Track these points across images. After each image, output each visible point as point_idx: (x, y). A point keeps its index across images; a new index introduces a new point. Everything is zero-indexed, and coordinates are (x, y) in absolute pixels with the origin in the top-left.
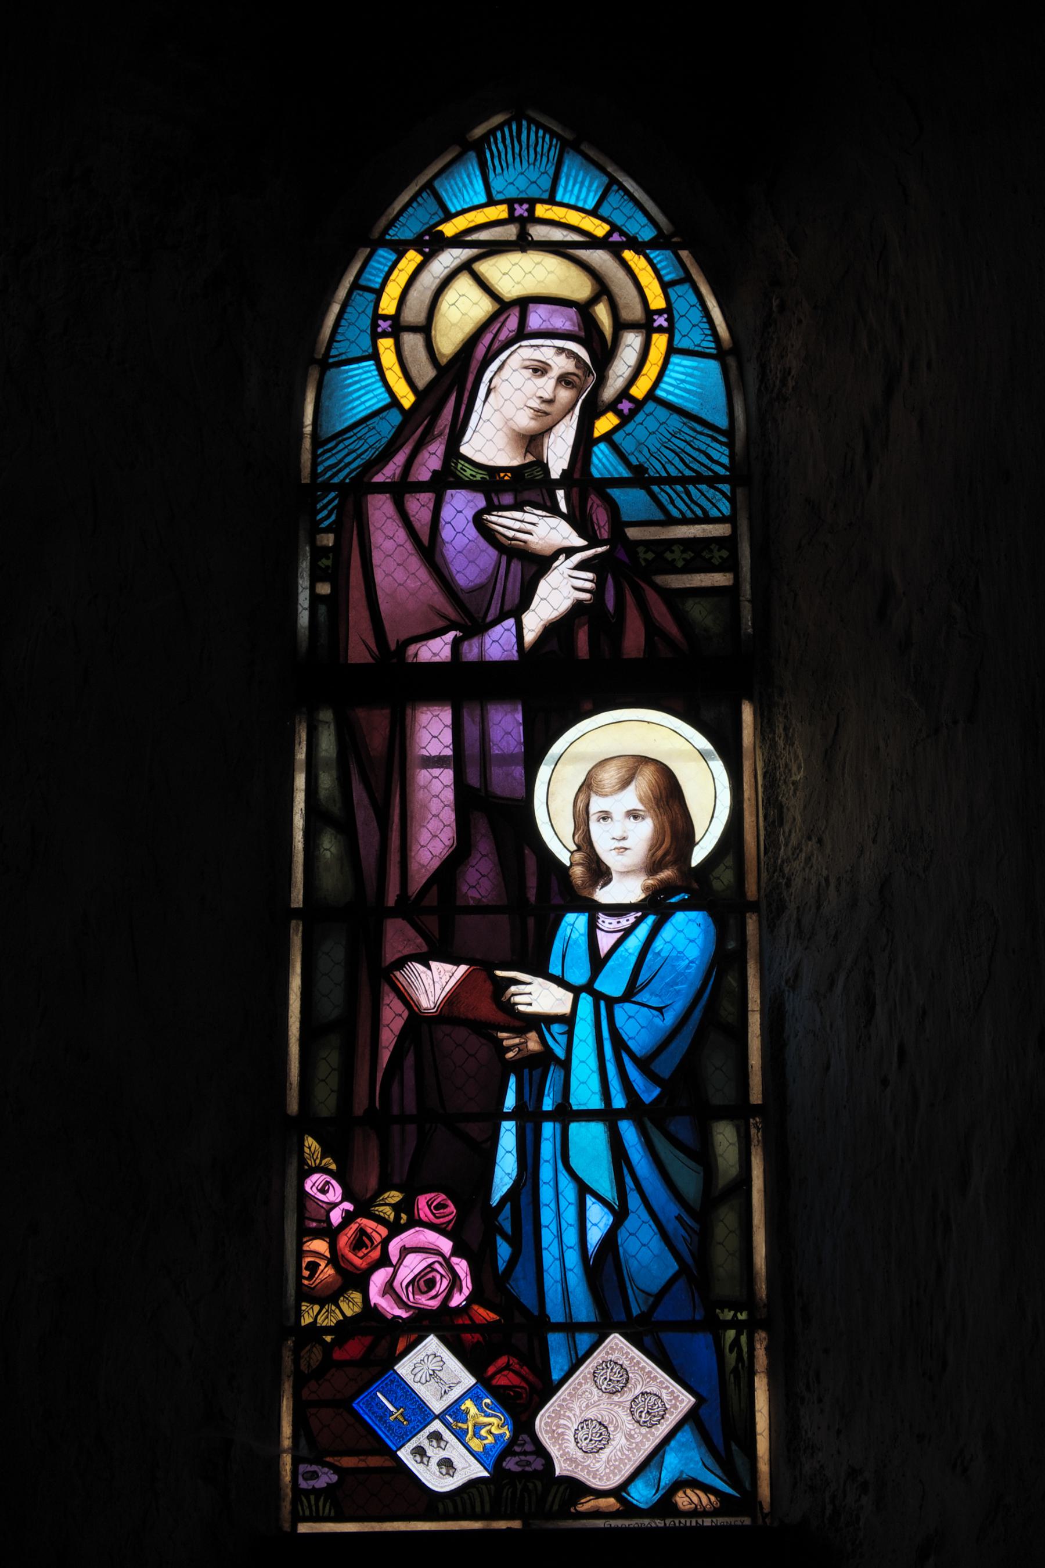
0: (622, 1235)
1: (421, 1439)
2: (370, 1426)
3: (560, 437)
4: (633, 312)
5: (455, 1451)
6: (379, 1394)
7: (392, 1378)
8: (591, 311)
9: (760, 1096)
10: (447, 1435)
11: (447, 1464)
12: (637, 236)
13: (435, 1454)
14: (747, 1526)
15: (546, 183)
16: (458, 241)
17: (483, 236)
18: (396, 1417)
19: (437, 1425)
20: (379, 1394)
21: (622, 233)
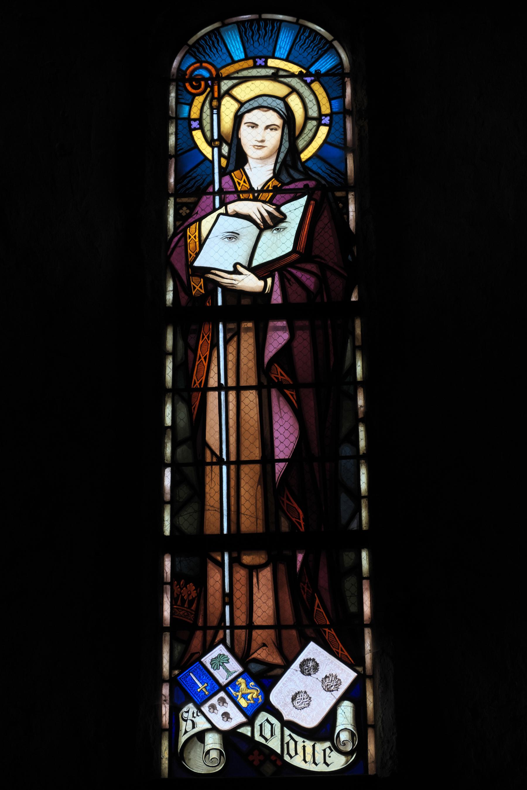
0: (295, 344)
1: (214, 700)
2: (194, 664)
3: (268, 51)
4: (313, 112)
5: (230, 708)
6: (191, 674)
7: (198, 666)
8: (242, 533)
9: (277, 182)
10: (228, 700)
11: (226, 716)
12: (287, 177)
13: (221, 709)
14: (364, 623)
15: (271, 48)
16: (229, 77)
17: (240, 75)
18: (202, 689)
19: (222, 694)
20: (191, 674)
21: (305, 82)
